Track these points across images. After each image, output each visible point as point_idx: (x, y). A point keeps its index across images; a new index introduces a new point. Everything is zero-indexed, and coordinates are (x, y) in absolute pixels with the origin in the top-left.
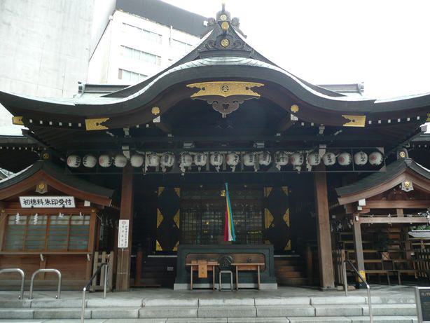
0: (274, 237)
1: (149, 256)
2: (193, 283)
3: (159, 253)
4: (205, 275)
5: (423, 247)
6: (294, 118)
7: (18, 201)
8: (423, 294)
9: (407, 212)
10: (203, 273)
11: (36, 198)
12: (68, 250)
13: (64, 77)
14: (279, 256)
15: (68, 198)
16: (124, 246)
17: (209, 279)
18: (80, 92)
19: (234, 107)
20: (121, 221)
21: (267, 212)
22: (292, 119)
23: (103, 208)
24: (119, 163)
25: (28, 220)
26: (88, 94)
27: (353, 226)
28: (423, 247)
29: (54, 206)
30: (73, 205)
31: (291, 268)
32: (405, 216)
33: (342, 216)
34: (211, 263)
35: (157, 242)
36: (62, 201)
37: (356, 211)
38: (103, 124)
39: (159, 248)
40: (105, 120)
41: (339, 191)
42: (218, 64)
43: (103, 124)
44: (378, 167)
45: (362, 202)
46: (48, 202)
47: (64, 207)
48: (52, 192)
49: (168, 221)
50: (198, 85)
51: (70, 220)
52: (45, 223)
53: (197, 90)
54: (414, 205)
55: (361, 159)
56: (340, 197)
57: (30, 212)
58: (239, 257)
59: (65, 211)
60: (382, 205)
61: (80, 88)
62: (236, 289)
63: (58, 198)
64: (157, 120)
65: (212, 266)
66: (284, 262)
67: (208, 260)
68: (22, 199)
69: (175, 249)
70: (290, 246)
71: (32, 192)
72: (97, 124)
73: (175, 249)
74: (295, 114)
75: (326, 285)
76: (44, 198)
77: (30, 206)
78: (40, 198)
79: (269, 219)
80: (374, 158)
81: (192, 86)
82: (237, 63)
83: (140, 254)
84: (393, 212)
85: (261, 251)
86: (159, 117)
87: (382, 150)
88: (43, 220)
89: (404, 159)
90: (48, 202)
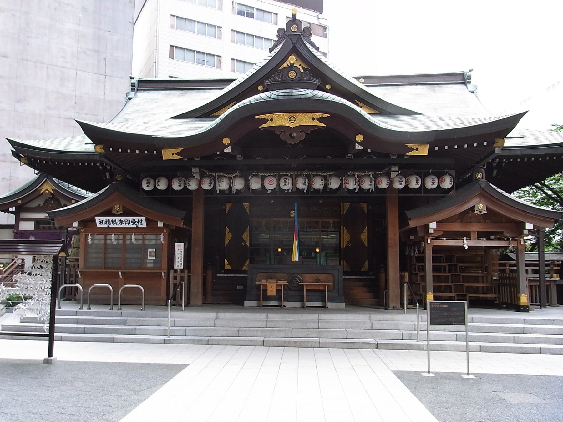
0: (349, 256)
1: (218, 275)
2: (263, 300)
3: (227, 272)
4: (274, 294)
5: (508, 271)
6: (358, 147)
7: (95, 221)
8: (432, 306)
9: (481, 235)
10: (272, 291)
11: (110, 218)
12: (105, 268)
13: (105, 59)
14: (354, 277)
15: (140, 218)
16: (180, 268)
17: (278, 297)
18: (133, 90)
19: (300, 137)
20: (176, 244)
21: (344, 231)
22: (356, 148)
23: (175, 228)
24: (193, 186)
25: (106, 239)
26: (142, 92)
27: (424, 248)
28: (508, 271)
29: (127, 226)
30: (144, 225)
31: (365, 289)
32: (478, 240)
33: (412, 240)
34: (280, 282)
35: (226, 261)
36: (134, 222)
37: (428, 234)
38: (177, 154)
39: (227, 267)
40: (179, 150)
41: (409, 213)
42: (285, 98)
43: (177, 154)
44: (448, 191)
45: (433, 225)
46: (121, 222)
47: (137, 226)
48: (126, 213)
49: (237, 238)
50: (266, 116)
51: (144, 239)
52: (121, 242)
53: (266, 121)
54: (483, 228)
55: (431, 184)
56: (410, 219)
57: (108, 231)
58: (308, 277)
59: (137, 230)
60: (457, 227)
61: (133, 85)
62: (304, 307)
63: (131, 218)
64: (228, 150)
65: (281, 285)
66: (358, 283)
67: (278, 280)
68: (98, 219)
69: (245, 268)
70: (367, 266)
71: (109, 213)
72: (173, 154)
73: (245, 268)
74: (360, 144)
75: (392, 305)
76: (117, 219)
77: (106, 226)
78: (114, 218)
79: (346, 237)
80: (442, 182)
81: (260, 117)
82: (303, 97)
83: (210, 273)
84: (468, 235)
85: (330, 272)
86: (230, 147)
87: (453, 172)
88: (118, 239)
89: (478, 180)
90: (121, 222)
